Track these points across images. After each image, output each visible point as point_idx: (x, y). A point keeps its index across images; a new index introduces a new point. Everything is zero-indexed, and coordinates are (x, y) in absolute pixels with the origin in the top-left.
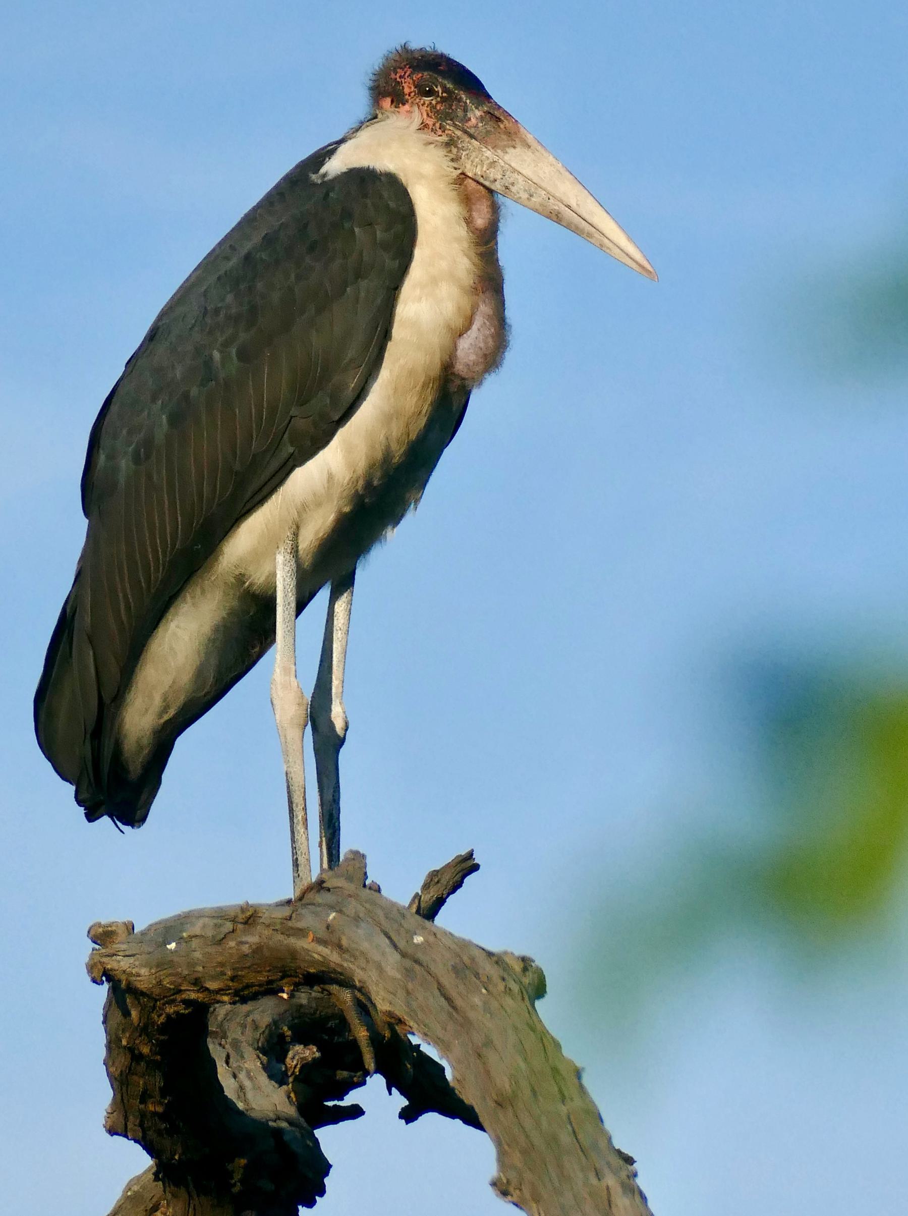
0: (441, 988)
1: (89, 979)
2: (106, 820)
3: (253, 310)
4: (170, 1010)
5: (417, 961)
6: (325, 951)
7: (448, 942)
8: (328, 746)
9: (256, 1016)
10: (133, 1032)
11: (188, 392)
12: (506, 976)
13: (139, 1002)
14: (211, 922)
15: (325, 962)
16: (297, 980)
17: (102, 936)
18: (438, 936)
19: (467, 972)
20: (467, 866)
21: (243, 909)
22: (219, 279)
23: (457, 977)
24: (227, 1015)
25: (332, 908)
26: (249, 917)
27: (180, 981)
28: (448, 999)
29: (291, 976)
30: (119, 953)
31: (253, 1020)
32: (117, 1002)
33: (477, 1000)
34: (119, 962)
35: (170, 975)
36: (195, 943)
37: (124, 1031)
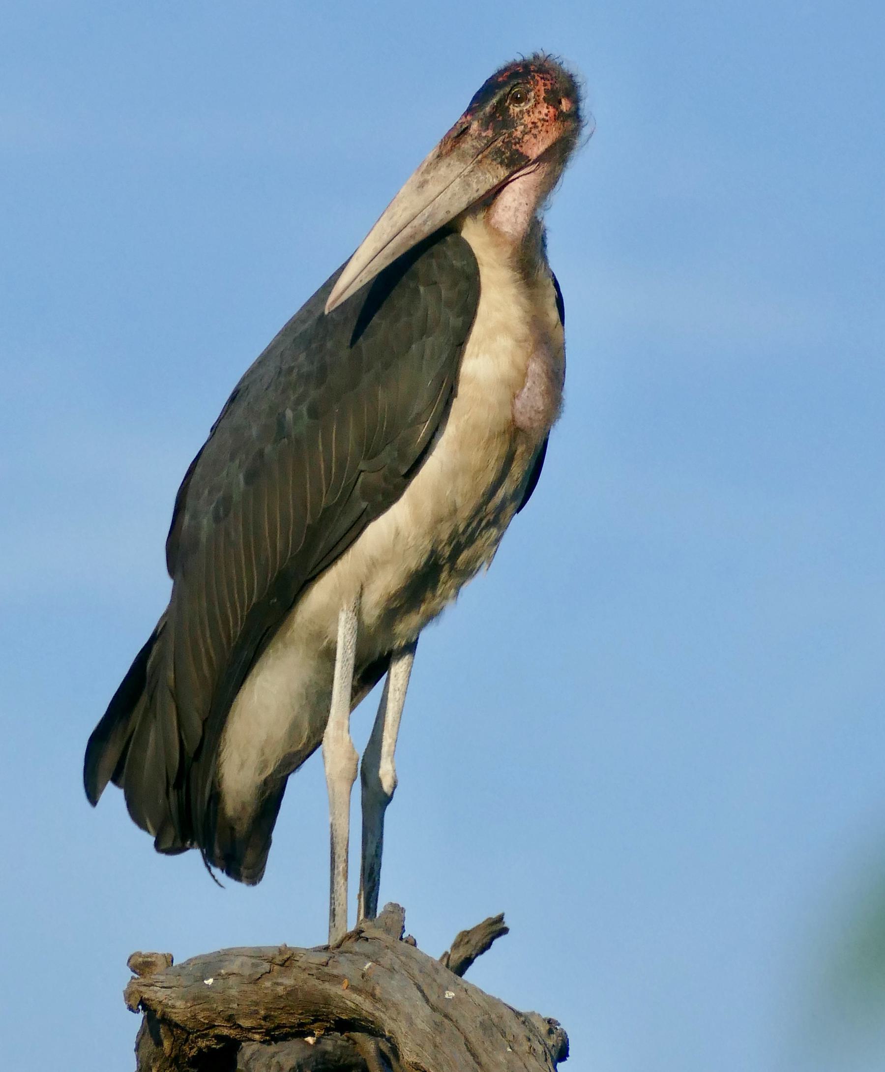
0: (467, 1042)
1: (126, 1006)
2: (194, 856)
3: (323, 370)
4: (202, 1043)
5: (446, 1016)
6: (359, 999)
7: (478, 999)
8: (376, 802)
9: (281, 1058)
10: (164, 1062)
11: (263, 449)
12: (531, 1037)
13: (172, 1034)
14: (250, 961)
15: (357, 1009)
16: (328, 1025)
17: (142, 966)
18: (469, 993)
19: (494, 1029)
20: (496, 929)
21: (281, 951)
22: (294, 340)
23: (485, 1034)
24: (253, 1054)
25: (368, 957)
26: (286, 960)
27: (214, 1016)
28: (474, 1055)
29: (322, 1021)
30: (157, 984)
31: (278, 1062)
32: (151, 1031)
33: (501, 1058)
34: (156, 992)
35: (207, 1010)
36: (232, 980)
37: (155, 1060)
